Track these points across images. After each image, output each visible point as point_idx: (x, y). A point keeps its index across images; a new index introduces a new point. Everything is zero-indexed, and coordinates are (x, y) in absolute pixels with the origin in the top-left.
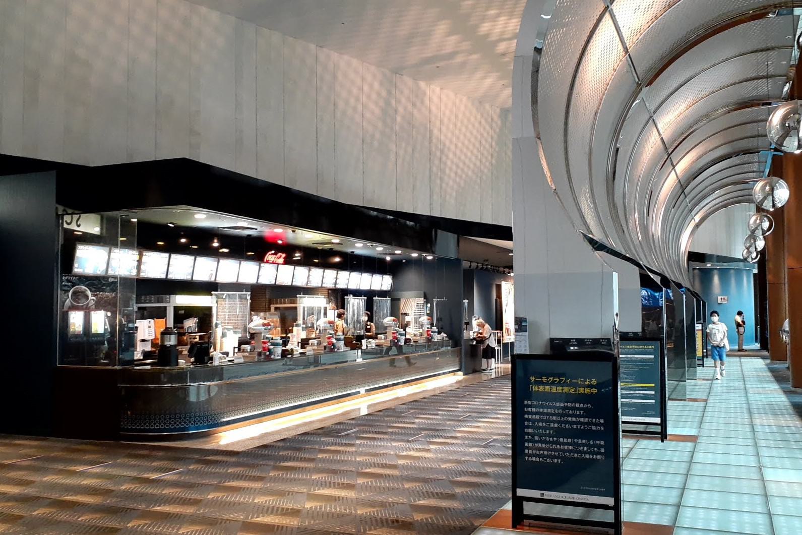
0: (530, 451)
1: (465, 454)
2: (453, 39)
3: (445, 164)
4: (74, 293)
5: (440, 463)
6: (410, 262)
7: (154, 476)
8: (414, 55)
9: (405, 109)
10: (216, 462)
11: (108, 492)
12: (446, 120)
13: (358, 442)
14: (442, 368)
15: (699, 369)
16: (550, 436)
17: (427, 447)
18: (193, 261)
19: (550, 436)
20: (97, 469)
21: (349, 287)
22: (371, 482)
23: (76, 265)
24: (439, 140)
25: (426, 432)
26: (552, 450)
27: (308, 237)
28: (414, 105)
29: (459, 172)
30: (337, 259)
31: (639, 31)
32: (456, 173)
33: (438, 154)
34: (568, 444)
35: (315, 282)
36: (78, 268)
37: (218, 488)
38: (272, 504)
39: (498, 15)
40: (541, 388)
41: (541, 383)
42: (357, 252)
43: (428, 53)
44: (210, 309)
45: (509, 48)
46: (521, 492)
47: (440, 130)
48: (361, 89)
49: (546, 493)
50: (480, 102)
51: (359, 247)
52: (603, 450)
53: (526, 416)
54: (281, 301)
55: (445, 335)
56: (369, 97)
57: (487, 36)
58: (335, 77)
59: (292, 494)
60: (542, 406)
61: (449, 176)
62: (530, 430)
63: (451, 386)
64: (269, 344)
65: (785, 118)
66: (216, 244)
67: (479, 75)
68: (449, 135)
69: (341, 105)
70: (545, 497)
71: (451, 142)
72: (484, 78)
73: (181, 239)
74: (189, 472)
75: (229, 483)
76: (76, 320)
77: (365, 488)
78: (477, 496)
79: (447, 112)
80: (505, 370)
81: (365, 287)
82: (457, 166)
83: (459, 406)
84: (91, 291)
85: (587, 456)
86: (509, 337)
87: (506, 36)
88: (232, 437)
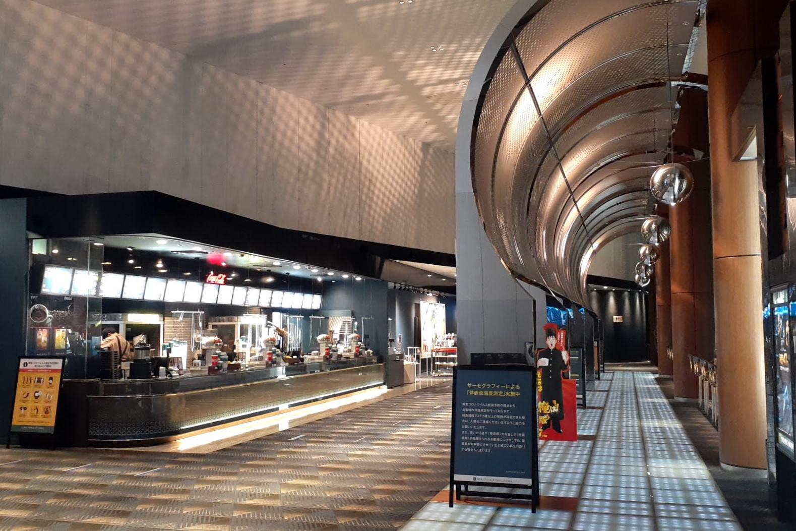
0: (466, 444)
1: (405, 452)
2: (385, 82)
3: (373, 192)
6: (340, 283)
7: (138, 474)
8: (347, 93)
9: (337, 141)
10: (187, 463)
11: (103, 486)
12: (374, 153)
13: (242, 470)
14: (369, 382)
15: (597, 382)
16: (482, 430)
17: (370, 448)
18: (123, 280)
19: (482, 430)
20: (81, 470)
22: (331, 474)
23: (44, 286)
24: (367, 169)
25: (366, 436)
26: (483, 442)
27: (251, 260)
28: (345, 138)
29: (386, 200)
30: (270, 280)
32: (383, 201)
33: (367, 183)
34: (496, 437)
36: (45, 288)
37: (199, 482)
38: (201, 514)
39: (425, 65)
40: (476, 393)
41: (477, 389)
42: (292, 273)
43: (361, 92)
44: (158, 326)
45: (434, 91)
46: (457, 477)
47: (369, 161)
48: (297, 123)
49: (477, 477)
50: (404, 136)
51: (296, 269)
52: (523, 441)
53: (464, 415)
54: (214, 319)
55: (371, 351)
56: (304, 129)
57: (415, 81)
58: (273, 110)
59: (215, 505)
60: (477, 407)
62: (466, 427)
63: (379, 398)
64: (219, 359)
65: (664, 177)
66: (160, 265)
67: (405, 113)
68: (377, 165)
69: (279, 136)
70: (477, 481)
71: (378, 171)
72: (409, 116)
73: (130, 259)
75: (89, 520)
76: (42, 336)
77: (325, 478)
78: (395, 502)
79: (375, 145)
80: (423, 384)
81: (297, 306)
82: (384, 194)
84: (49, 309)
86: (427, 353)
87: (431, 82)
88: (184, 444)
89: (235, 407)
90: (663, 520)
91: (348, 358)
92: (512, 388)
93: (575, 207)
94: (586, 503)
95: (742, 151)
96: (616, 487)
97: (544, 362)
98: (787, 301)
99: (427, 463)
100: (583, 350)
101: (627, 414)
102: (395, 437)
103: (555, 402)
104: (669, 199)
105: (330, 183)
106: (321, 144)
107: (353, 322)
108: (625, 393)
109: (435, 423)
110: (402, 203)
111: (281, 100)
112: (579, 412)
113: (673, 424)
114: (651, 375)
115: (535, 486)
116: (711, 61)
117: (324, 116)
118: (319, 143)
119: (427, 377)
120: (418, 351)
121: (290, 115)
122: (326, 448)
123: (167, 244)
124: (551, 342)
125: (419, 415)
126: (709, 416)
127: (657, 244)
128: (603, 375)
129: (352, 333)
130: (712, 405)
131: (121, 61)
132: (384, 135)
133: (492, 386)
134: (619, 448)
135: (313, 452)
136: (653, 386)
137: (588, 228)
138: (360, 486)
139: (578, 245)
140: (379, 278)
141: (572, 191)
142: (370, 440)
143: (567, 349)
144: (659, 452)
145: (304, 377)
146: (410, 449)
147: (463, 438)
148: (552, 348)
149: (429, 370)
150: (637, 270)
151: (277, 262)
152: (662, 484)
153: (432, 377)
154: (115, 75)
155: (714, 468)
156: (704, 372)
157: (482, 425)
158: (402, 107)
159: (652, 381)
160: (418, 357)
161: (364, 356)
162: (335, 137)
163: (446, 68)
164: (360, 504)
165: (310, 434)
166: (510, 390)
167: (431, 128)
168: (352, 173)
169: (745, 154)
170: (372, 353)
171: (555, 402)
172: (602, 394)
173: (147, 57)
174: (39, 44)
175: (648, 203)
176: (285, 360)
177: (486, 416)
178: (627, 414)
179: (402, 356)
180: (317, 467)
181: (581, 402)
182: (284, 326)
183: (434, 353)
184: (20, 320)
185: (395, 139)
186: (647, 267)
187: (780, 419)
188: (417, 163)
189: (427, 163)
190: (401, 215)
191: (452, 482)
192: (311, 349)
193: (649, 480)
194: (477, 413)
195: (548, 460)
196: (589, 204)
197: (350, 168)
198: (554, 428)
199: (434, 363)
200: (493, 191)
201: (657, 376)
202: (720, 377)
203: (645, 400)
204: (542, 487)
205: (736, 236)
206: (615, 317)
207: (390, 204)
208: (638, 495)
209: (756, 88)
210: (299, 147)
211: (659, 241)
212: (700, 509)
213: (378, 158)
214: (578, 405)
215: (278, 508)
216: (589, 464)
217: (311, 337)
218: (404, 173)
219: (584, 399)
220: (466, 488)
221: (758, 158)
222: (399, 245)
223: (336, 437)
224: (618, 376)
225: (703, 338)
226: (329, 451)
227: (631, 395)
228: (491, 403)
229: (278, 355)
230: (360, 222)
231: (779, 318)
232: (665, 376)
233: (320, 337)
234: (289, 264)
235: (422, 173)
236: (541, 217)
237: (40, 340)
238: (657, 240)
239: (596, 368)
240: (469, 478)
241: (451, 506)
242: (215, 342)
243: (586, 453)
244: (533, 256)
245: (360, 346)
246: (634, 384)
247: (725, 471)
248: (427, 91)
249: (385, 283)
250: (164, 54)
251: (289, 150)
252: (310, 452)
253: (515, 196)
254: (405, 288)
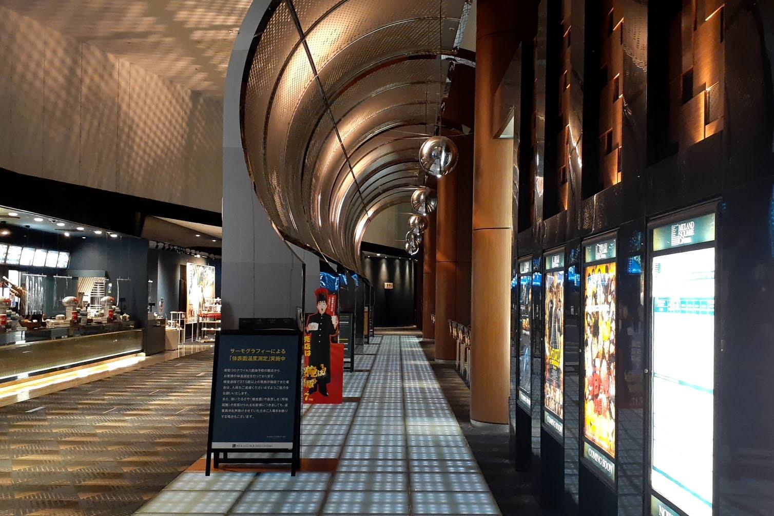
0: (227, 411)
1: (160, 422)
2: (149, 20)
3: (133, 141)
5: (138, 431)
8: (105, 27)
9: (92, 79)
12: (135, 96)
14: (124, 348)
15: (365, 346)
16: (244, 396)
17: (122, 418)
19: (244, 396)
21: (21, 264)
24: (126, 114)
28: (102, 77)
29: (148, 150)
31: (326, 58)
32: (145, 151)
33: (126, 130)
34: (259, 402)
39: (196, 7)
40: (240, 358)
42: (33, 226)
43: (122, 29)
46: (215, 445)
47: (129, 106)
48: (43, 54)
50: (171, 82)
51: (38, 222)
53: (225, 382)
55: (128, 316)
57: (183, 23)
61: (137, 154)
62: (228, 393)
63: (136, 365)
65: (432, 149)
67: (172, 56)
68: (139, 111)
69: (20, 68)
71: (140, 118)
72: (177, 60)
77: (66, 453)
79: (137, 89)
80: (186, 350)
81: (39, 263)
83: (147, 383)
85: (274, 411)
86: (193, 318)
87: (201, 26)
90: (416, 475)
91: (100, 323)
92: (278, 352)
93: (351, 173)
94: (346, 463)
95: (501, 130)
96: (375, 446)
97: (314, 326)
98: (531, 271)
99: (185, 432)
100: (353, 315)
101: (391, 376)
102: (151, 407)
103: (322, 365)
104: (436, 171)
106: (72, 81)
107: (107, 283)
108: (391, 356)
109: (196, 392)
110: (166, 154)
111: (23, 27)
112: (346, 375)
113: (432, 385)
114: (416, 339)
115: (296, 449)
116: (479, 39)
117: (77, 51)
118: (69, 81)
119: (191, 344)
120: (183, 316)
121: (33, 45)
122: (71, 420)
124: (322, 307)
125: (179, 383)
126: (464, 377)
127: (425, 214)
128: (372, 340)
129: (105, 296)
130: (466, 366)
132: (148, 79)
133: (256, 351)
134: (381, 409)
135: (54, 425)
136: (417, 349)
137: (364, 195)
138: (106, 459)
139: (353, 210)
140: (139, 236)
141: (348, 156)
142: (122, 410)
143: (336, 314)
144: (416, 411)
145: (48, 343)
146: (166, 418)
147: (223, 405)
148: (322, 313)
149: (195, 336)
150: (407, 238)
152: (418, 440)
153: (198, 343)
155: (464, 425)
156: (461, 336)
157: (245, 391)
158: (169, 51)
159: (417, 344)
160: (182, 323)
161: (119, 321)
162: (89, 74)
163: (218, 12)
164: (106, 478)
165: (52, 405)
166: (276, 355)
167: (201, 76)
169: (503, 133)
170: (129, 318)
171: (322, 365)
172: (370, 358)
175: (419, 173)
176: (23, 325)
177: (249, 381)
178: (391, 376)
179: (163, 322)
180: (57, 441)
181: (349, 365)
182: (23, 285)
183: (201, 318)
185: (160, 84)
186: (416, 237)
187: (521, 378)
188: (186, 113)
189: (197, 114)
190: (166, 167)
191: (210, 450)
192: (55, 312)
193: (406, 436)
194: (240, 379)
195: (312, 423)
196: (365, 171)
197: (107, 112)
198: (320, 391)
199: (200, 329)
200: (265, 148)
201: (421, 340)
202: (473, 341)
203: (409, 362)
204: (303, 450)
205: (493, 210)
206: (386, 284)
208: (395, 453)
209: (516, 68)
210: (44, 82)
211: (426, 212)
212: (450, 463)
213: (141, 103)
214: (345, 368)
215: (8, 487)
216: (351, 425)
217: (55, 298)
219: (352, 362)
220: (225, 455)
221: (515, 138)
222: (162, 200)
223: (83, 409)
224: (386, 340)
225: (462, 307)
227: (396, 358)
228: (255, 369)
229: (14, 319)
230: (118, 172)
231: (524, 287)
232: (428, 340)
233: (66, 299)
234: (28, 215)
235: (191, 123)
236: (317, 178)
238: (425, 210)
239: (365, 333)
240: (228, 445)
241: (208, 474)
243: (349, 414)
244: (307, 221)
245: (114, 310)
246: (400, 347)
247: (473, 426)
248: (197, 35)
249: (146, 242)
252: (50, 425)
253: (288, 156)
254: (169, 248)
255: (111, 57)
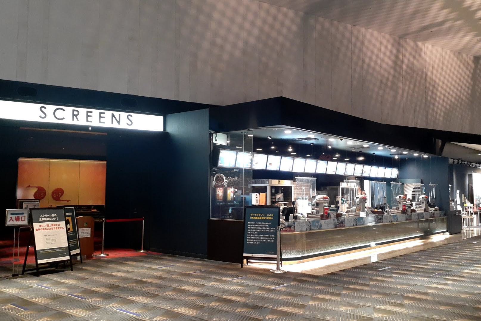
3: (436, 94)
4: (217, 178)
6: (412, 160)
7: (272, 287)
8: (416, 25)
9: (409, 60)
12: (436, 66)
13: (344, 292)
20: (237, 280)
23: (220, 162)
24: (431, 79)
27: (349, 143)
28: (414, 57)
29: (446, 99)
30: (361, 159)
32: (443, 101)
35: (350, 172)
37: (313, 299)
42: (377, 153)
43: (427, 22)
47: (432, 73)
48: (379, 50)
50: (459, 53)
51: (380, 150)
56: (385, 54)
57: (470, 7)
58: (363, 43)
60: (254, 224)
61: (439, 103)
66: (290, 149)
67: (460, 35)
68: (438, 75)
71: (440, 79)
74: (291, 286)
76: (220, 192)
77: (410, 307)
81: (381, 176)
82: (444, 95)
89: (339, 243)
105: (403, 90)
110: (458, 101)
111: (368, 36)
117: (399, 44)
118: (395, 62)
121: (374, 45)
123: (293, 133)
131: (265, 21)
132: (444, 54)
135: (397, 282)
151: (366, 145)
154: (261, 30)
158: (459, 30)
162: (407, 58)
168: (420, 83)
173: (280, 17)
174: (216, 15)
184: (207, 183)
185: (452, 56)
188: (470, 71)
197: (419, 79)
207: (449, 102)
213: (440, 70)
218: (460, 80)
223: (415, 271)
226: (410, 282)
237: (219, 195)
242: (324, 198)
250: (291, 14)
251: (374, 69)
255: (420, 44)
